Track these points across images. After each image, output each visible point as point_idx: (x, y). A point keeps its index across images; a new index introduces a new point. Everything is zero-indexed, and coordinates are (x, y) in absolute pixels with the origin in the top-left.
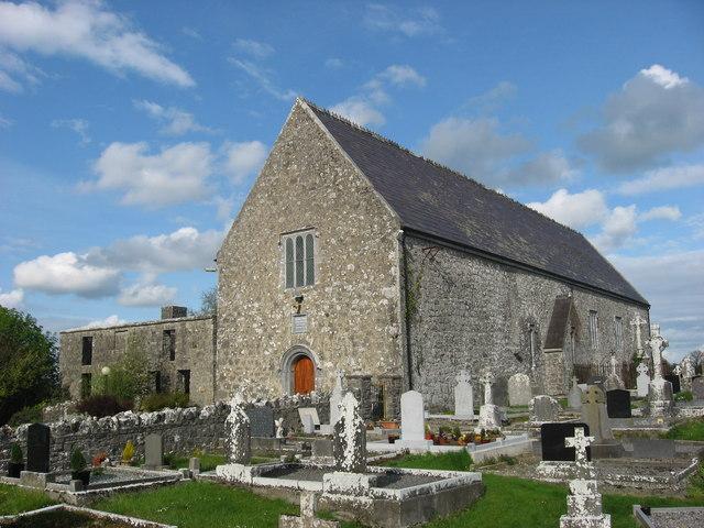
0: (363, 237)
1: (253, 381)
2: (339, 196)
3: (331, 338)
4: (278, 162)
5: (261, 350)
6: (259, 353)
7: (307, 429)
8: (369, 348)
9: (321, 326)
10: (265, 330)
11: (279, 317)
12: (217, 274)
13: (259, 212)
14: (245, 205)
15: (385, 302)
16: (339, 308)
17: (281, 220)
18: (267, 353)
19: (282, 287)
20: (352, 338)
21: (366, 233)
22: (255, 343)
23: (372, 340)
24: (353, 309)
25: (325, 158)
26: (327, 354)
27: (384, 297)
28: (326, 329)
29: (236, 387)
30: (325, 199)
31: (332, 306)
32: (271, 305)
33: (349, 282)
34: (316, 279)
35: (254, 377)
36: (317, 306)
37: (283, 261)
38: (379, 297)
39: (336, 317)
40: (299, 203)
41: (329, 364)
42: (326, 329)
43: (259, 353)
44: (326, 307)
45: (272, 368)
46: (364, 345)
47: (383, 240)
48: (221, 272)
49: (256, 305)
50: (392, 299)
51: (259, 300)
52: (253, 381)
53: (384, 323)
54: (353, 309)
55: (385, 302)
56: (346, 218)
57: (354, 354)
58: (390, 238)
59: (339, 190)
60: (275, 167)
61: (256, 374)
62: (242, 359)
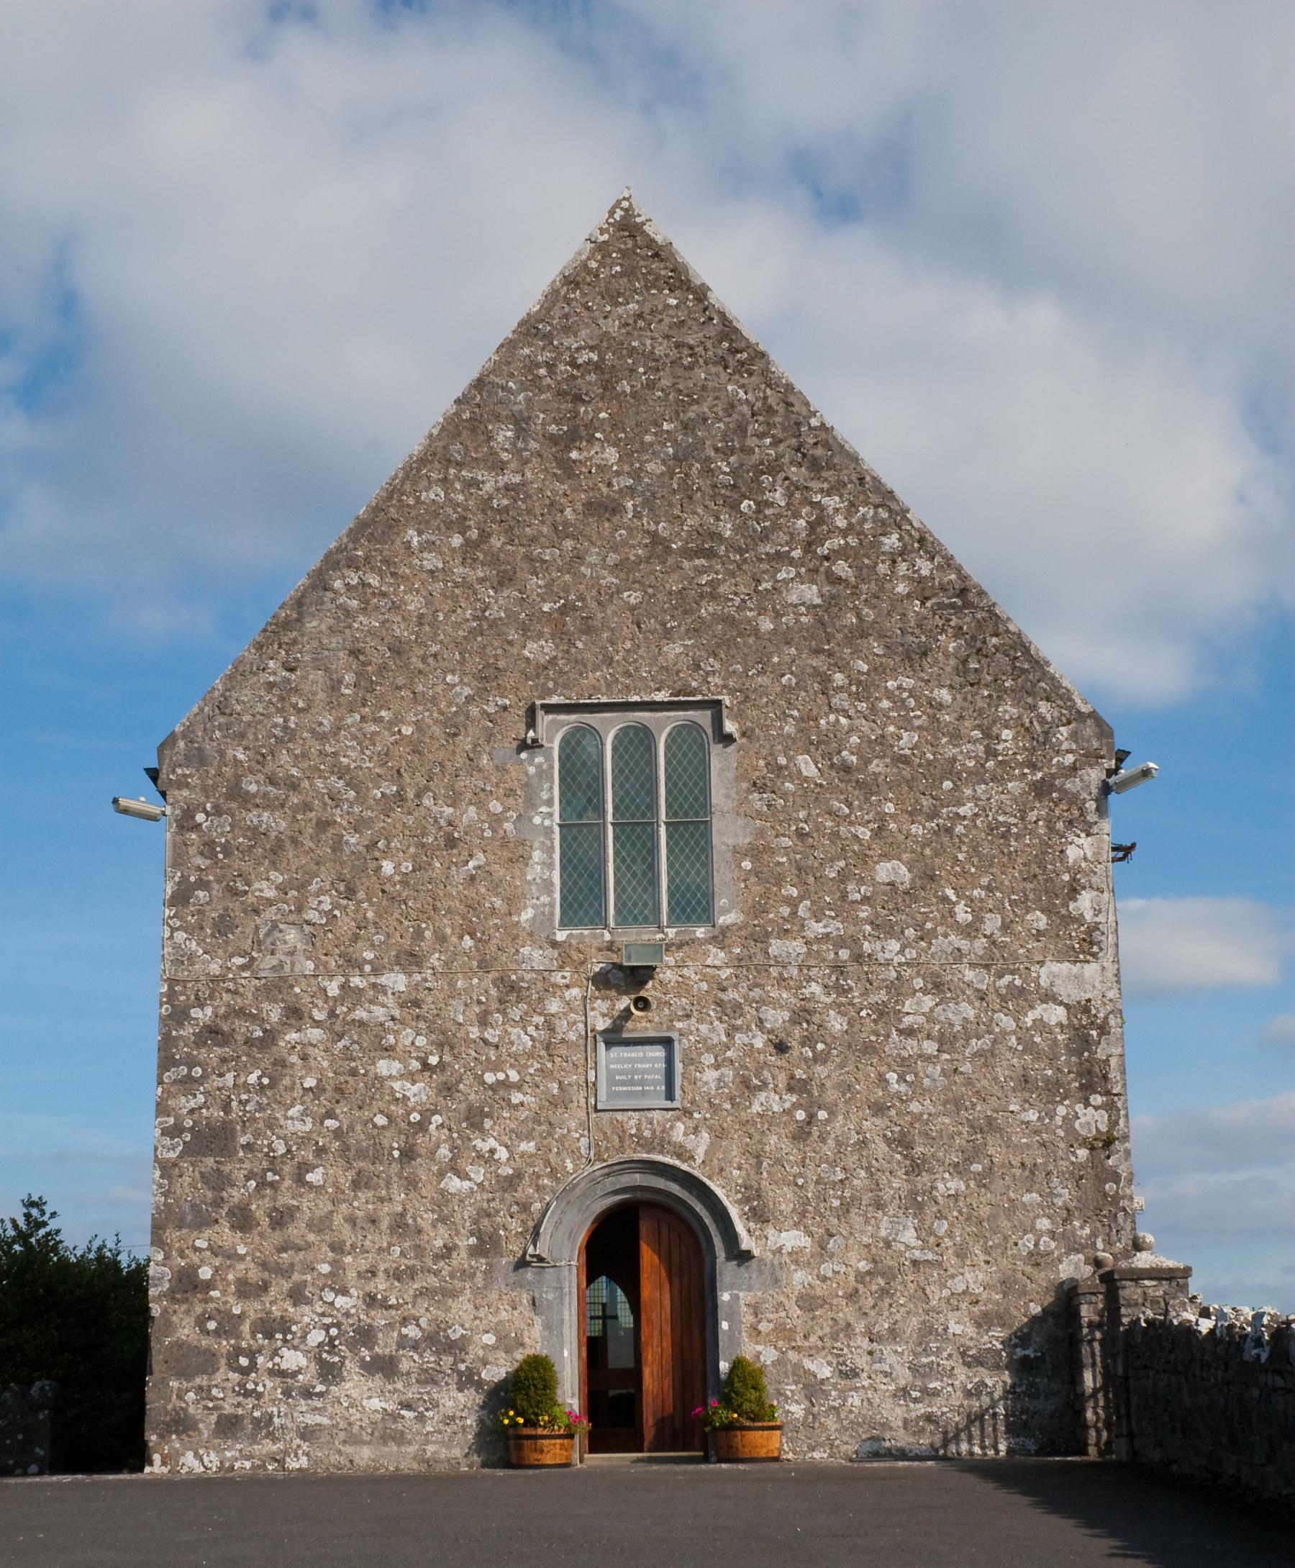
0: (950, 770)
1: (371, 1301)
2: (831, 603)
3: (801, 1134)
4: (521, 424)
5: (421, 1169)
6: (412, 1184)
7: (346, 572)
8: (983, 1181)
9: (748, 1087)
10: (448, 1090)
11: (522, 1040)
12: (165, 833)
13: (415, 604)
14: (333, 562)
15: (1056, 1014)
16: (837, 1024)
17: (539, 649)
18: (454, 1184)
19: (543, 918)
20: (902, 1142)
21: (967, 753)
22: (395, 1144)
23: (995, 1150)
24: (909, 1032)
25: (765, 449)
26: (783, 1199)
27: (1049, 997)
28: (771, 1101)
29: (529, 511)
30: (768, 601)
31: (803, 1014)
32: (484, 986)
33: (885, 929)
34: (722, 902)
35: (380, 1285)
36: (730, 1011)
37: (549, 815)
38: (1020, 997)
39: (819, 1059)
40: (633, 597)
41: (792, 1239)
42: (771, 1101)
43: (412, 1184)
44: (776, 1018)
45: (486, 1245)
46: (958, 1170)
47: (1041, 790)
48: (186, 822)
49: (397, 981)
50: (1085, 1008)
51: (411, 960)
52: (371, 1301)
53: (1053, 1091)
54: (909, 1032)
55: (1056, 1014)
56: (864, 688)
57: (915, 1204)
58: (1072, 785)
59: (834, 580)
60: (505, 434)
61: (397, 1275)
62: (308, 1205)
